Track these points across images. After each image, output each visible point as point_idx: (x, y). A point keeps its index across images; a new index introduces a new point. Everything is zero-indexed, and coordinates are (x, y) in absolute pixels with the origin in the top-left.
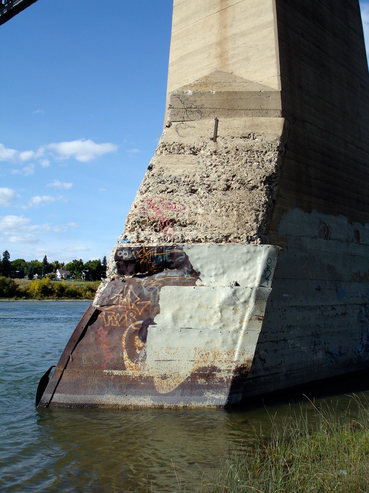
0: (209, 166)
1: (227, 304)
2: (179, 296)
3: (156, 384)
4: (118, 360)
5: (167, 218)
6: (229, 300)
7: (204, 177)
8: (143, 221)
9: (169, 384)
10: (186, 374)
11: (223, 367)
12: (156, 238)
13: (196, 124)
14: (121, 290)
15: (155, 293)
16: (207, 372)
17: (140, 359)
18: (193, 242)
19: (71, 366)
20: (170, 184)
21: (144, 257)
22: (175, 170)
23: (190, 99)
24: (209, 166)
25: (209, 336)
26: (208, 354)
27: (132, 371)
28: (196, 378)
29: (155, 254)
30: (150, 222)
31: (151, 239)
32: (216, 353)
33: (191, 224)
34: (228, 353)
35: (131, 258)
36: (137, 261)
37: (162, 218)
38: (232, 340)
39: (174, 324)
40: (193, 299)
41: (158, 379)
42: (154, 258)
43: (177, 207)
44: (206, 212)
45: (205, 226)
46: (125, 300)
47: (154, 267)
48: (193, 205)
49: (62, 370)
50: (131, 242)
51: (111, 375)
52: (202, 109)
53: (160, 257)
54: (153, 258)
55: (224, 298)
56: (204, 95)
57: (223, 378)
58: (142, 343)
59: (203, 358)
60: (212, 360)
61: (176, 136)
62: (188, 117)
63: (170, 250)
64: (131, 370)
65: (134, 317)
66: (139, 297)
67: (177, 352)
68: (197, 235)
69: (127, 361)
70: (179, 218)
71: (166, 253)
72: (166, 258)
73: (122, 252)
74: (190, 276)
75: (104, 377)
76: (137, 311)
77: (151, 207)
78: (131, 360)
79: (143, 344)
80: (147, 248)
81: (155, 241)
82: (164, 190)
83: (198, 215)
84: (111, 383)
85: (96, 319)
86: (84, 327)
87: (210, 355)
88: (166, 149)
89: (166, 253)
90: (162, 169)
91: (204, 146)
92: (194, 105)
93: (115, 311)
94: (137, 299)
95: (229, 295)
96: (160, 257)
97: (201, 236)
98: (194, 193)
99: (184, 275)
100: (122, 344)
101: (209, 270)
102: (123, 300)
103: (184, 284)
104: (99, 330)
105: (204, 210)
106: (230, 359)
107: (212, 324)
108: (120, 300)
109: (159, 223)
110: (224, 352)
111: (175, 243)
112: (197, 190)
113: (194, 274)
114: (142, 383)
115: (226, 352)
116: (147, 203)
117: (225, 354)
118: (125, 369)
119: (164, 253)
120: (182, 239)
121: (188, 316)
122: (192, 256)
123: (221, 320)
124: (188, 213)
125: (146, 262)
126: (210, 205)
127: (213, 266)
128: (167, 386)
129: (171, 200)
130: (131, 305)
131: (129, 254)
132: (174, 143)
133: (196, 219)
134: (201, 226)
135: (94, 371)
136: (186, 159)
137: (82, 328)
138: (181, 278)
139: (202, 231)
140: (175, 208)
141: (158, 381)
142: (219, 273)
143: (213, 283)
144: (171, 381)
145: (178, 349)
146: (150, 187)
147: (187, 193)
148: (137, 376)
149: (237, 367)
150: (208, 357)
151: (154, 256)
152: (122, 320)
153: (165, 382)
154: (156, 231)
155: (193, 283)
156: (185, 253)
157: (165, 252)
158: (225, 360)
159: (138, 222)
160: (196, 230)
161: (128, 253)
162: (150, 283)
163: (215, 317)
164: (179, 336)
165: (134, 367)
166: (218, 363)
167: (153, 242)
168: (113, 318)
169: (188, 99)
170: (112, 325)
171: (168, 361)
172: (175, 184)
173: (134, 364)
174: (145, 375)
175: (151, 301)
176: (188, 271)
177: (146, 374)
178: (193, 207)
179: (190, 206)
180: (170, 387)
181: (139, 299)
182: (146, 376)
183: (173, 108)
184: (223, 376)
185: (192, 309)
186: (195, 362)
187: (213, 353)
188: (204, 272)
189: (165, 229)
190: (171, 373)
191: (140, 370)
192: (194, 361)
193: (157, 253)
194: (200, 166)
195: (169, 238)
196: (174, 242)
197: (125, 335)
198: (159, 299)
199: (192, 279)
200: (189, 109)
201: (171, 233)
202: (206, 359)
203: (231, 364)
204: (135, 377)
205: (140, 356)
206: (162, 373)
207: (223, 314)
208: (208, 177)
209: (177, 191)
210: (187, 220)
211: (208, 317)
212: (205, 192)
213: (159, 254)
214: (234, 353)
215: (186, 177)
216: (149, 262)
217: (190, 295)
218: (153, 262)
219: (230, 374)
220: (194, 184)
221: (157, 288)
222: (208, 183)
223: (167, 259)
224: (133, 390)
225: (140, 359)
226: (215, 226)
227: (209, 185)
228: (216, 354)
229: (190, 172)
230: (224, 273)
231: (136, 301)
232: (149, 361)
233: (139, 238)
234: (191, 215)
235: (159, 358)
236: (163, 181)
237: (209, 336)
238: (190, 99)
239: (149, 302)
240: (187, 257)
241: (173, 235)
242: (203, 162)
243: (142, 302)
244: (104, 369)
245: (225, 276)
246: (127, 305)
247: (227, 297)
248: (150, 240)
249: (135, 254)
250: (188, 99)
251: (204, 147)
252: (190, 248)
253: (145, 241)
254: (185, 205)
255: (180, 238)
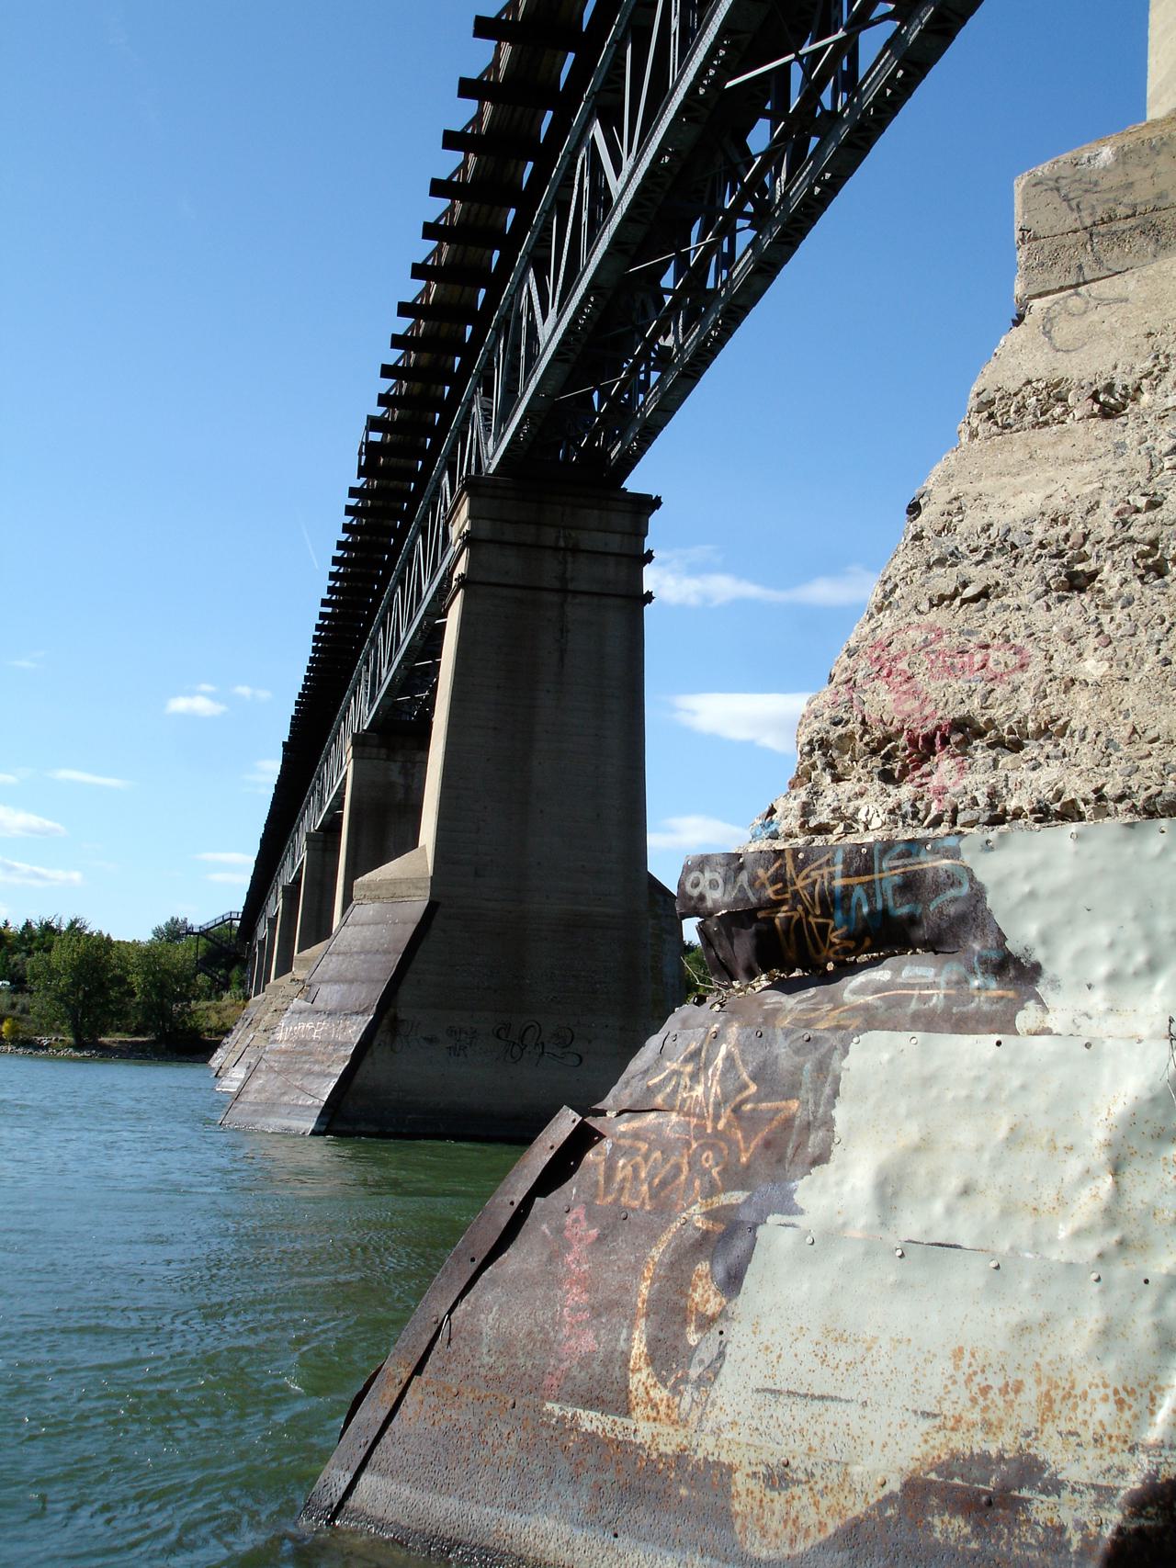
0: (1167, 455)
1: (1148, 1129)
2: (927, 1081)
3: (737, 1507)
4: (608, 1361)
5: (940, 714)
6: (1160, 1112)
7: (1138, 511)
8: (840, 737)
9: (793, 1514)
10: (879, 1480)
11: (1076, 1467)
12: (881, 812)
13: (1132, 285)
14: (693, 1046)
15: (822, 1067)
16: (986, 1482)
17: (694, 1373)
18: (1038, 821)
19: (439, 1364)
20: (978, 563)
21: (788, 896)
22: (1012, 501)
23: (1105, 184)
24: (1167, 455)
25: (1035, 1294)
26: (1017, 1391)
27: (652, 1424)
28: (923, 1509)
29: (839, 883)
30: (867, 738)
31: (861, 816)
32: (1057, 1387)
33: (1043, 732)
34: (1123, 1395)
35: (736, 900)
36: (761, 915)
37: (917, 715)
38: (1158, 1327)
39: (877, 1221)
40: (988, 1099)
41: (751, 1484)
42: (833, 901)
43: (991, 664)
44: (1116, 672)
45: (1103, 738)
46: (699, 1090)
47: (836, 941)
48: (1062, 645)
49: (405, 1375)
50: (780, 831)
51: (571, 1429)
52: (1158, 214)
53: (859, 893)
54: (830, 902)
55: (1129, 1101)
56: (1165, 149)
57: (1061, 1529)
58: (718, 1300)
59: (985, 1409)
60: (1029, 1420)
61: (1038, 354)
62: (1098, 261)
63: (906, 861)
64: (648, 1418)
65: (715, 1172)
66: (754, 1079)
67: (868, 1362)
68: (1060, 785)
69: (638, 1376)
70: (991, 713)
71: (885, 874)
72: (884, 900)
73: (701, 876)
74: (993, 984)
75: (545, 1434)
76: (732, 1143)
77: (884, 672)
78: (658, 1375)
79: (724, 1300)
80: (801, 856)
81: (876, 823)
82: (947, 593)
83: (1077, 687)
84: (564, 1466)
85: (573, 1170)
86: (518, 1199)
87: (1023, 1397)
88: (991, 416)
89: (885, 874)
90: (956, 504)
91: (1156, 369)
92: (1126, 206)
93: (653, 1137)
94: (745, 1087)
95: (1160, 1085)
96: (859, 893)
97: (1078, 788)
98: (1082, 590)
99: (967, 982)
100: (638, 1294)
101: (1082, 955)
102: (691, 1089)
103: (961, 1024)
104: (569, 1220)
105: (1107, 665)
106: (1124, 1430)
107: (1063, 1232)
108: (680, 1090)
109: (902, 741)
110: (1102, 1390)
111: (958, 828)
112: (1093, 576)
113: (1012, 973)
114: (683, 1492)
115: (1110, 1391)
116: (870, 657)
117: (1105, 1399)
118: (627, 1413)
119: (876, 876)
120: (992, 806)
121: (953, 1183)
122: (1000, 884)
123: (1111, 1215)
124: (1033, 685)
125: (800, 920)
126: (1142, 637)
127: (1102, 933)
128: (786, 1522)
129: (970, 633)
130: (717, 1118)
131: (725, 883)
132: (1029, 382)
133: (1068, 706)
134: (1083, 739)
135: (511, 1402)
136: (1068, 442)
137: (512, 1203)
138: (952, 992)
139: (1087, 763)
140: (984, 666)
141: (749, 1492)
142: (1130, 969)
143: (1094, 1022)
144: (805, 1500)
145: (876, 1347)
146: (896, 586)
147: (1046, 592)
148: (668, 1450)
149: (1153, 1476)
150: (1010, 1404)
151: (832, 892)
152: (664, 1184)
153: (778, 1500)
154: (887, 777)
155: (1002, 1023)
156: (969, 870)
157: (881, 871)
158: (1100, 1431)
159: (824, 744)
160: (1058, 762)
161: (720, 881)
162: (813, 1015)
163: (1085, 1195)
164: (892, 1278)
165: (662, 1408)
166: (1056, 1442)
167: (867, 829)
168: (636, 1169)
169: (1096, 184)
170: (622, 1199)
171: (813, 1397)
172: (1002, 560)
173: (665, 1393)
174: (700, 1454)
175: (802, 1103)
176: (984, 961)
177: (706, 1447)
178: (1063, 652)
179: (1052, 650)
180: (798, 1530)
181: (753, 1088)
182: (705, 1459)
183: (1036, 239)
184: (1066, 1517)
185: (980, 1149)
186: (937, 1422)
187: (1044, 1387)
188: (1059, 964)
189: (926, 768)
190: (812, 1460)
191: (685, 1424)
192: (935, 1416)
193: (846, 875)
194: (1122, 464)
195: (934, 806)
196: (954, 822)
197: (656, 1253)
198: (836, 1093)
199: (1002, 998)
200: (1103, 229)
201: (948, 783)
202: (1001, 1414)
203: (1122, 1459)
204: (660, 1455)
205: (695, 1360)
206: (775, 1452)
207: (1126, 1181)
208: (1153, 505)
209: (1005, 591)
210: (1026, 717)
211: (1048, 1195)
212: (1130, 576)
213: (854, 880)
214: (1153, 1399)
215: (1055, 520)
216: (812, 920)
217: (978, 1079)
218: (830, 916)
219: (1103, 1514)
220: (1087, 548)
221: (834, 1039)
222: (1150, 534)
223: (891, 903)
224: (643, 1517)
225: (694, 1373)
226: (1151, 734)
227: (1154, 544)
228: (1057, 1395)
229: (1073, 497)
230: (1153, 967)
231: (739, 1098)
232: (732, 1391)
233: (813, 813)
234: (1048, 690)
235: (777, 1379)
236: (952, 554)
237: (1035, 1294)
238: (1105, 184)
239: (794, 1105)
240: (978, 894)
241: (952, 790)
242: (1143, 441)
243: (764, 1105)
244: (549, 1400)
245: (1161, 983)
246: (701, 1116)
247: (1148, 1095)
248: (856, 821)
249: (751, 885)
250: (1096, 184)
251: (1156, 373)
252: (992, 849)
253: (835, 827)
254: (1030, 648)
255: (983, 800)
